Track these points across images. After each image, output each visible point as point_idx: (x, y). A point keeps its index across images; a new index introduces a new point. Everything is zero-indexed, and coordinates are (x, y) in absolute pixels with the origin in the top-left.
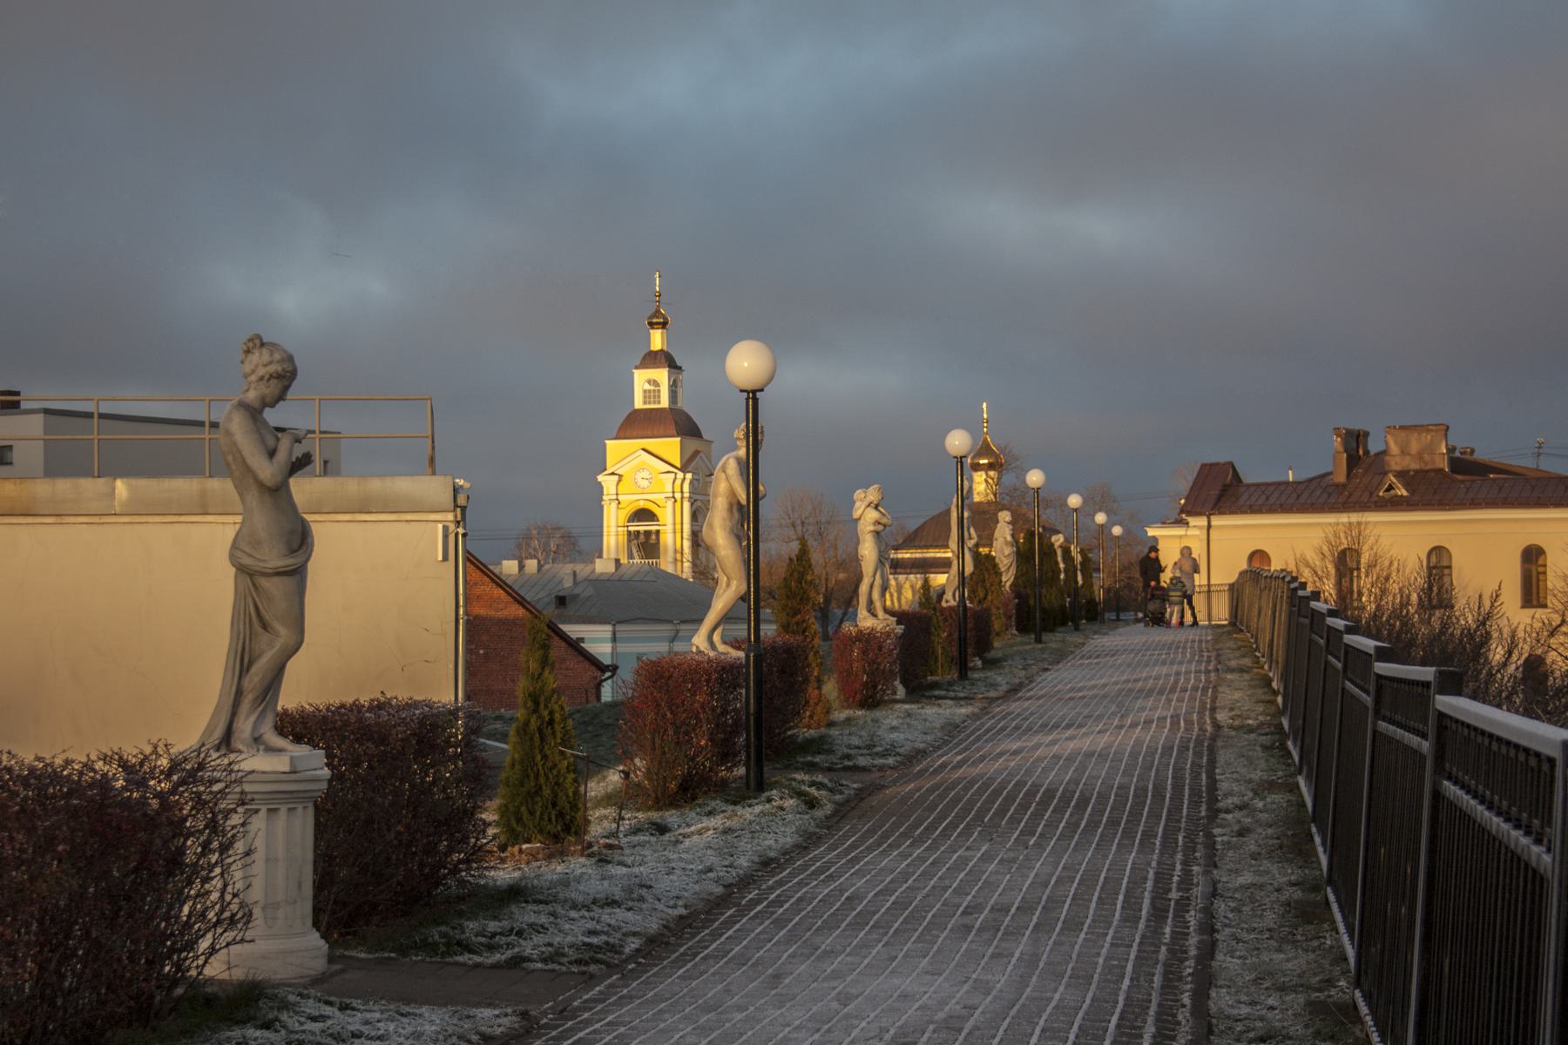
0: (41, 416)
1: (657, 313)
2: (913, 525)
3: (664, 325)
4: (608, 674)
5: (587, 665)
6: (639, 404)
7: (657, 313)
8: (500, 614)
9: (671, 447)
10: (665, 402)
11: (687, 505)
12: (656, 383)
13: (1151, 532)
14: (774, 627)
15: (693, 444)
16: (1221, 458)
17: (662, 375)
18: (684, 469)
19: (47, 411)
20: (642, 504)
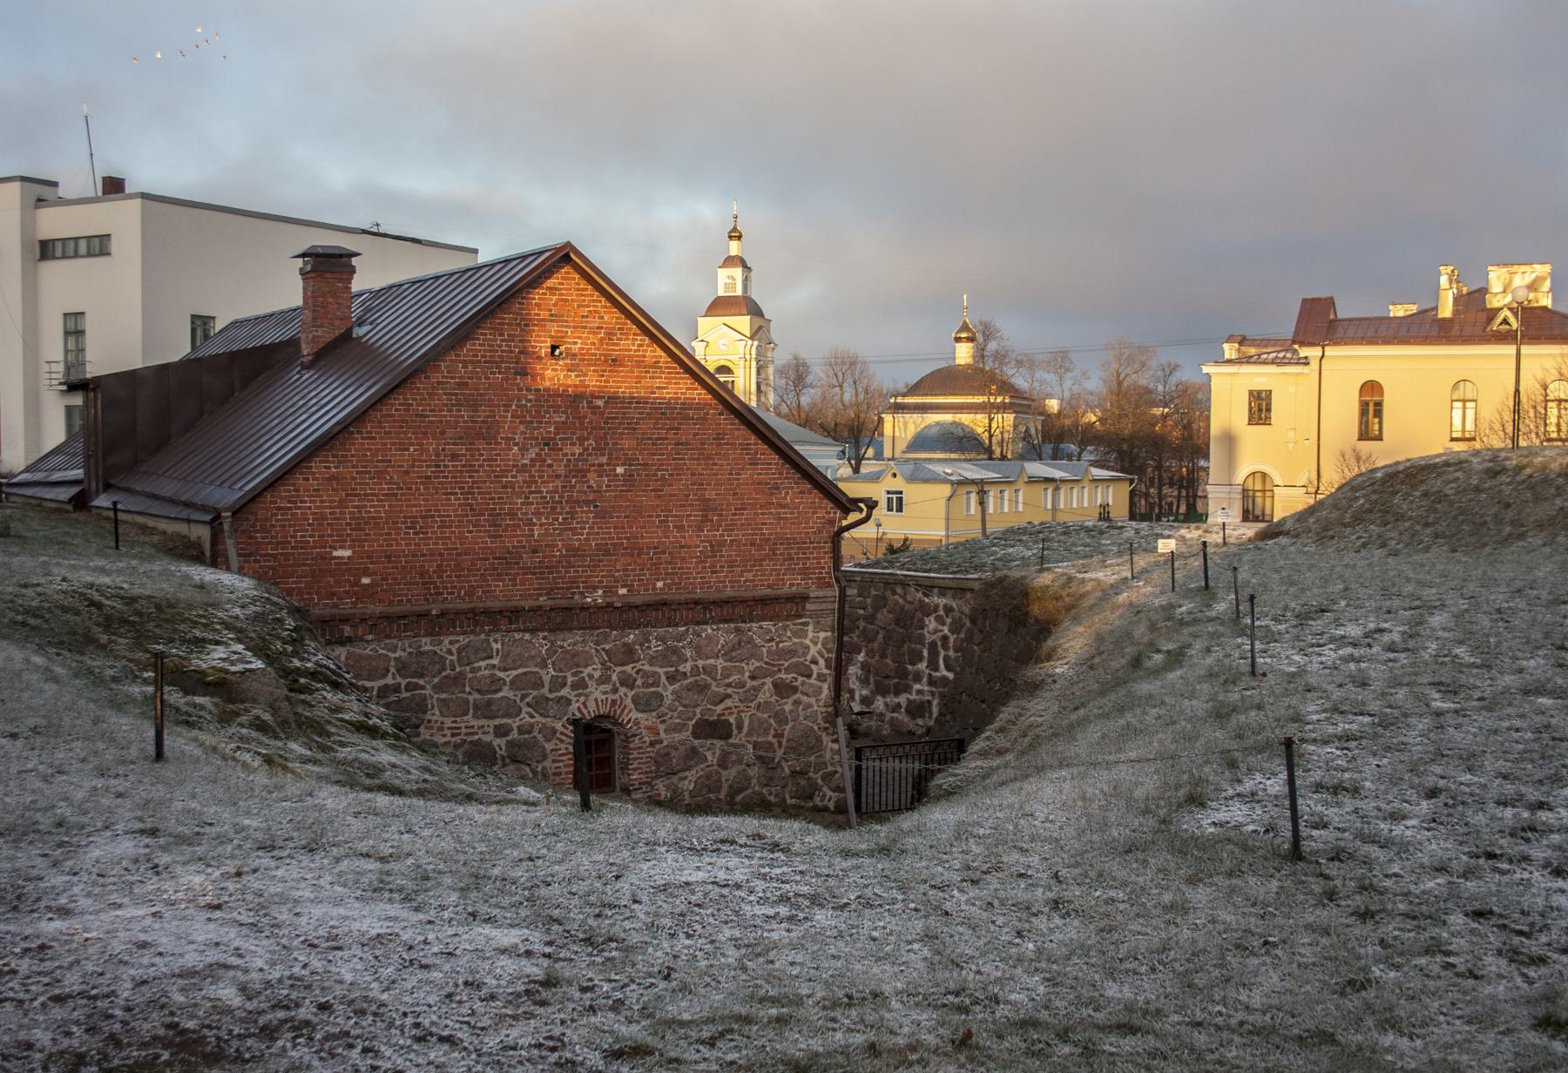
0: (18, 184)
1: (735, 229)
2: (914, 380)
3: (739, 238)
4: (854, 517)
5: (816, 497)
6: (721, 293)
7: (735, 229)
8: (711, 819)
9: (744, 323)
10: (739, 292)
11: (754, 363)
12: (733, 278)
13: (1206, 369)
14: (96, 503)
15: (758, 322)
16: (1323, 295)
17: (737, 272)
18: (752, 338)
19: (23, 179)
20: (722, 363)
